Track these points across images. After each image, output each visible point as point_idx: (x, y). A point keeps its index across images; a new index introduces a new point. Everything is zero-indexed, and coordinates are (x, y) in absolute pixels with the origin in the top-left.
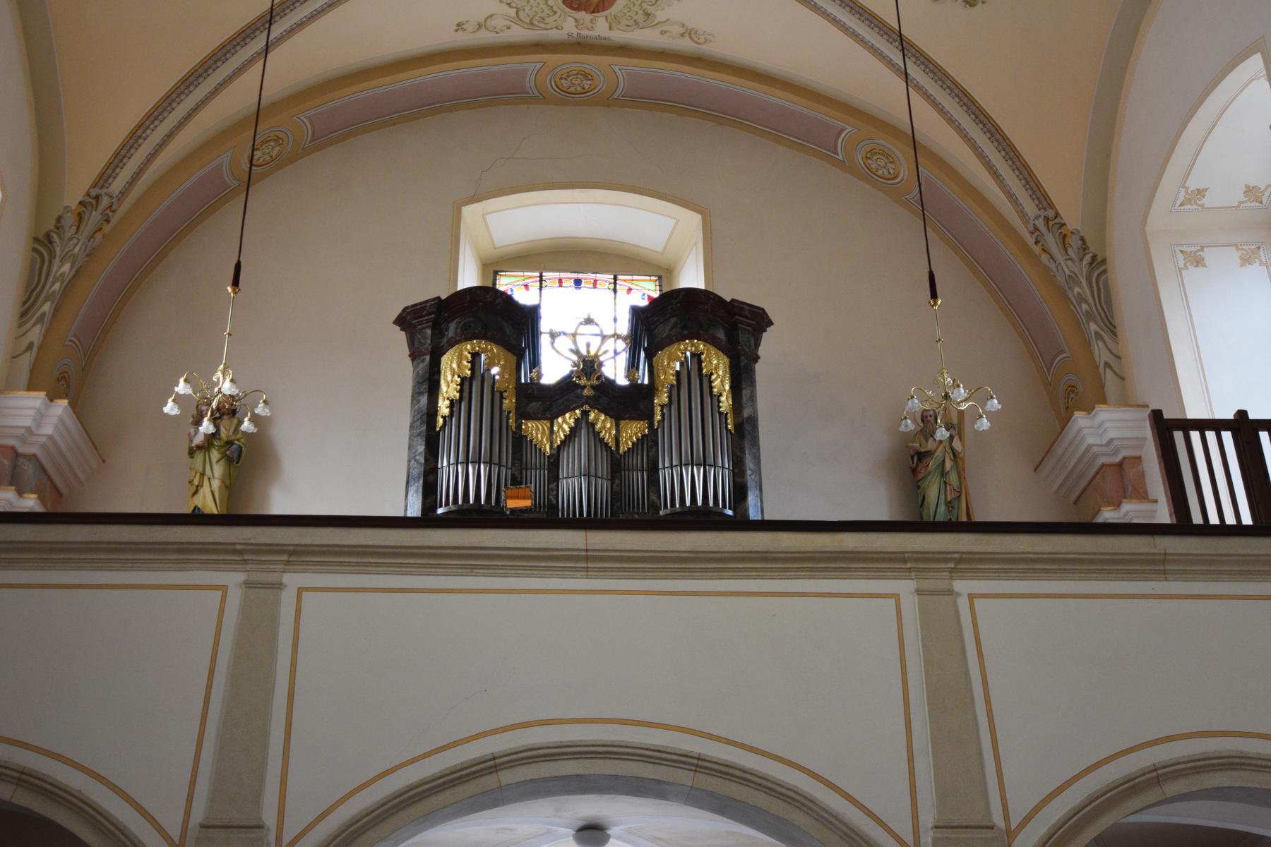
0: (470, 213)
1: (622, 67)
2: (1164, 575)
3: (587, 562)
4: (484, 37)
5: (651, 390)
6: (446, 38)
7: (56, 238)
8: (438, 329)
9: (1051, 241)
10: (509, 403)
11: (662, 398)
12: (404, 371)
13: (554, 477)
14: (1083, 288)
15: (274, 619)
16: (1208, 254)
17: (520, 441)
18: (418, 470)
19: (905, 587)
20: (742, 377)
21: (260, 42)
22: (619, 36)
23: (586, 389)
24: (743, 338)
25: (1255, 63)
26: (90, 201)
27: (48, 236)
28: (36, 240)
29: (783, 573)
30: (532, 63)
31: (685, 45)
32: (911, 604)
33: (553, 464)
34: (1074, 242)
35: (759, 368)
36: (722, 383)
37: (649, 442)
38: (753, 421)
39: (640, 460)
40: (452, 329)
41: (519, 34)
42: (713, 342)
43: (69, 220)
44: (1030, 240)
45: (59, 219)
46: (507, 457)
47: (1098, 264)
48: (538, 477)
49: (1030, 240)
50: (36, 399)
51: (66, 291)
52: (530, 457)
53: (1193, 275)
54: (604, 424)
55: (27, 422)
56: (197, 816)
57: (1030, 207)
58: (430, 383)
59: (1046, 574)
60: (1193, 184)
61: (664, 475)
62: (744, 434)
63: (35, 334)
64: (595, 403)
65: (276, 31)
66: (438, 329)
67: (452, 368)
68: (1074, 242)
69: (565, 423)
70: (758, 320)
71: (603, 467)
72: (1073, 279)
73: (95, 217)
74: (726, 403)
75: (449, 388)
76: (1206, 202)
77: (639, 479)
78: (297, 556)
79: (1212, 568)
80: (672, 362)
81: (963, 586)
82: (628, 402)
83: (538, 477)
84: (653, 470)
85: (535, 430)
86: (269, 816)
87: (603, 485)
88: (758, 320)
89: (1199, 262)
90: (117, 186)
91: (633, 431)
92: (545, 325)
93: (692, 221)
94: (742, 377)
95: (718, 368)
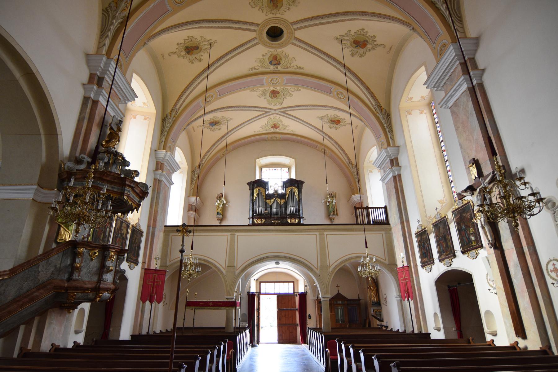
0: (257, 160)
1: (281, 136)
2: (353, 231)
3: (275, 231)
4: (259, 133)
5: (285, 195)
6: (253, 133)
7: (109, 10)
8: (253, 185)
9: (350, 165)
10: (264, 197)
11: (287, 196)
12: (248, 192)
13: (271, 209)
14: (355, 174)
15: (234, 239)
16: (413, 112)
17: (266, 203)
18: (251, 208)
19: (317, 233)
20: (300, 192)
21: (206, 74)
22: (280, 131)
23: (276, 195)
24: (300, 185)
25: (423, 68)
26: (172, 110)
27: (107, 9)
28: (103, 10)
29: (301, 232)
30: (267, 136)
31: (291, 132)
32: (318, 236)
33: (271, 207)
34: (384, 111)
35: (302, 190)
36: (296, 193)
37: (285, 203)
38: (301, 199)
39: (284, 206)
40: (255, 185)
41: (264, 132)
42: (295, 187)
43: (169, 115)
44: (374, 110)
45: (110, 4)
46: (264, 206)
47: (357, 170)
48: (269, 209)
49: (374, 110)
50: (195, 197)
51: (169, 130)
52: (268, 206)
53: (370, 174)
54: (278, 200)
55: (162, 156)
56: (227, 265)
57: (347, 160)
58: (252, 194)
59: (337, 231)
60: (410, 96)
61: (288, 208)
62: (300, 201)
63: (193, 186)
64: (277, 197)
65: (210, 71)
66: (253, 185)
67: (256, 191)
68: (384, 111)
69: (273, 200)
70: (302, 183)
71: (279, 207)
72: (354, 172)
73: (173, 114)
74: (297, 196)
75: (255, 195)
76: (413, 100)
77: (284, 209)
78: (237, 231)
79: (438, 155)
80: (289, 190)
81: (325, 233)
82: (282, 196)
83: (269, 209)
84: (286, 207)
85: (268, 201)
86: (235, 265)
87: (279, 210)
88: (302, 183)
89: (371, 172)
90: (178, 107)
91: (283, 201)
92: (270, 185)
93: (293, 160)
94: (300, 192)
95: (296, 191)
